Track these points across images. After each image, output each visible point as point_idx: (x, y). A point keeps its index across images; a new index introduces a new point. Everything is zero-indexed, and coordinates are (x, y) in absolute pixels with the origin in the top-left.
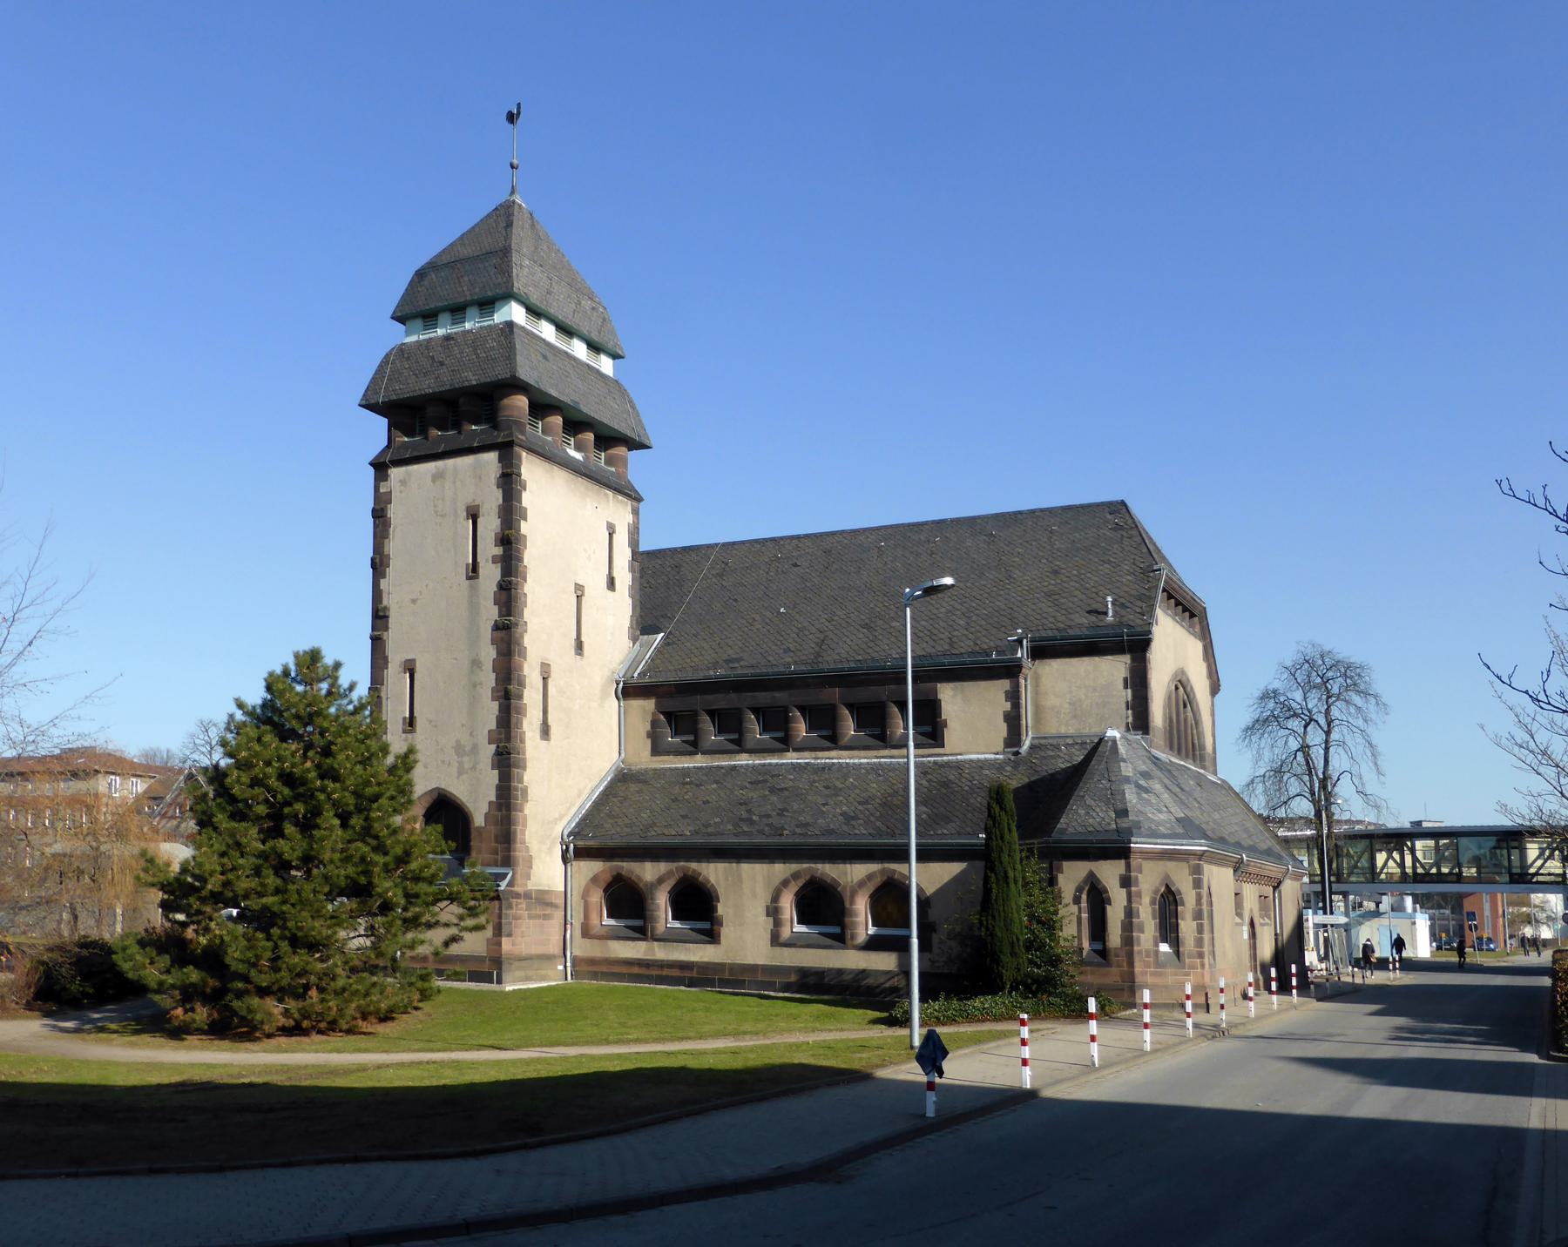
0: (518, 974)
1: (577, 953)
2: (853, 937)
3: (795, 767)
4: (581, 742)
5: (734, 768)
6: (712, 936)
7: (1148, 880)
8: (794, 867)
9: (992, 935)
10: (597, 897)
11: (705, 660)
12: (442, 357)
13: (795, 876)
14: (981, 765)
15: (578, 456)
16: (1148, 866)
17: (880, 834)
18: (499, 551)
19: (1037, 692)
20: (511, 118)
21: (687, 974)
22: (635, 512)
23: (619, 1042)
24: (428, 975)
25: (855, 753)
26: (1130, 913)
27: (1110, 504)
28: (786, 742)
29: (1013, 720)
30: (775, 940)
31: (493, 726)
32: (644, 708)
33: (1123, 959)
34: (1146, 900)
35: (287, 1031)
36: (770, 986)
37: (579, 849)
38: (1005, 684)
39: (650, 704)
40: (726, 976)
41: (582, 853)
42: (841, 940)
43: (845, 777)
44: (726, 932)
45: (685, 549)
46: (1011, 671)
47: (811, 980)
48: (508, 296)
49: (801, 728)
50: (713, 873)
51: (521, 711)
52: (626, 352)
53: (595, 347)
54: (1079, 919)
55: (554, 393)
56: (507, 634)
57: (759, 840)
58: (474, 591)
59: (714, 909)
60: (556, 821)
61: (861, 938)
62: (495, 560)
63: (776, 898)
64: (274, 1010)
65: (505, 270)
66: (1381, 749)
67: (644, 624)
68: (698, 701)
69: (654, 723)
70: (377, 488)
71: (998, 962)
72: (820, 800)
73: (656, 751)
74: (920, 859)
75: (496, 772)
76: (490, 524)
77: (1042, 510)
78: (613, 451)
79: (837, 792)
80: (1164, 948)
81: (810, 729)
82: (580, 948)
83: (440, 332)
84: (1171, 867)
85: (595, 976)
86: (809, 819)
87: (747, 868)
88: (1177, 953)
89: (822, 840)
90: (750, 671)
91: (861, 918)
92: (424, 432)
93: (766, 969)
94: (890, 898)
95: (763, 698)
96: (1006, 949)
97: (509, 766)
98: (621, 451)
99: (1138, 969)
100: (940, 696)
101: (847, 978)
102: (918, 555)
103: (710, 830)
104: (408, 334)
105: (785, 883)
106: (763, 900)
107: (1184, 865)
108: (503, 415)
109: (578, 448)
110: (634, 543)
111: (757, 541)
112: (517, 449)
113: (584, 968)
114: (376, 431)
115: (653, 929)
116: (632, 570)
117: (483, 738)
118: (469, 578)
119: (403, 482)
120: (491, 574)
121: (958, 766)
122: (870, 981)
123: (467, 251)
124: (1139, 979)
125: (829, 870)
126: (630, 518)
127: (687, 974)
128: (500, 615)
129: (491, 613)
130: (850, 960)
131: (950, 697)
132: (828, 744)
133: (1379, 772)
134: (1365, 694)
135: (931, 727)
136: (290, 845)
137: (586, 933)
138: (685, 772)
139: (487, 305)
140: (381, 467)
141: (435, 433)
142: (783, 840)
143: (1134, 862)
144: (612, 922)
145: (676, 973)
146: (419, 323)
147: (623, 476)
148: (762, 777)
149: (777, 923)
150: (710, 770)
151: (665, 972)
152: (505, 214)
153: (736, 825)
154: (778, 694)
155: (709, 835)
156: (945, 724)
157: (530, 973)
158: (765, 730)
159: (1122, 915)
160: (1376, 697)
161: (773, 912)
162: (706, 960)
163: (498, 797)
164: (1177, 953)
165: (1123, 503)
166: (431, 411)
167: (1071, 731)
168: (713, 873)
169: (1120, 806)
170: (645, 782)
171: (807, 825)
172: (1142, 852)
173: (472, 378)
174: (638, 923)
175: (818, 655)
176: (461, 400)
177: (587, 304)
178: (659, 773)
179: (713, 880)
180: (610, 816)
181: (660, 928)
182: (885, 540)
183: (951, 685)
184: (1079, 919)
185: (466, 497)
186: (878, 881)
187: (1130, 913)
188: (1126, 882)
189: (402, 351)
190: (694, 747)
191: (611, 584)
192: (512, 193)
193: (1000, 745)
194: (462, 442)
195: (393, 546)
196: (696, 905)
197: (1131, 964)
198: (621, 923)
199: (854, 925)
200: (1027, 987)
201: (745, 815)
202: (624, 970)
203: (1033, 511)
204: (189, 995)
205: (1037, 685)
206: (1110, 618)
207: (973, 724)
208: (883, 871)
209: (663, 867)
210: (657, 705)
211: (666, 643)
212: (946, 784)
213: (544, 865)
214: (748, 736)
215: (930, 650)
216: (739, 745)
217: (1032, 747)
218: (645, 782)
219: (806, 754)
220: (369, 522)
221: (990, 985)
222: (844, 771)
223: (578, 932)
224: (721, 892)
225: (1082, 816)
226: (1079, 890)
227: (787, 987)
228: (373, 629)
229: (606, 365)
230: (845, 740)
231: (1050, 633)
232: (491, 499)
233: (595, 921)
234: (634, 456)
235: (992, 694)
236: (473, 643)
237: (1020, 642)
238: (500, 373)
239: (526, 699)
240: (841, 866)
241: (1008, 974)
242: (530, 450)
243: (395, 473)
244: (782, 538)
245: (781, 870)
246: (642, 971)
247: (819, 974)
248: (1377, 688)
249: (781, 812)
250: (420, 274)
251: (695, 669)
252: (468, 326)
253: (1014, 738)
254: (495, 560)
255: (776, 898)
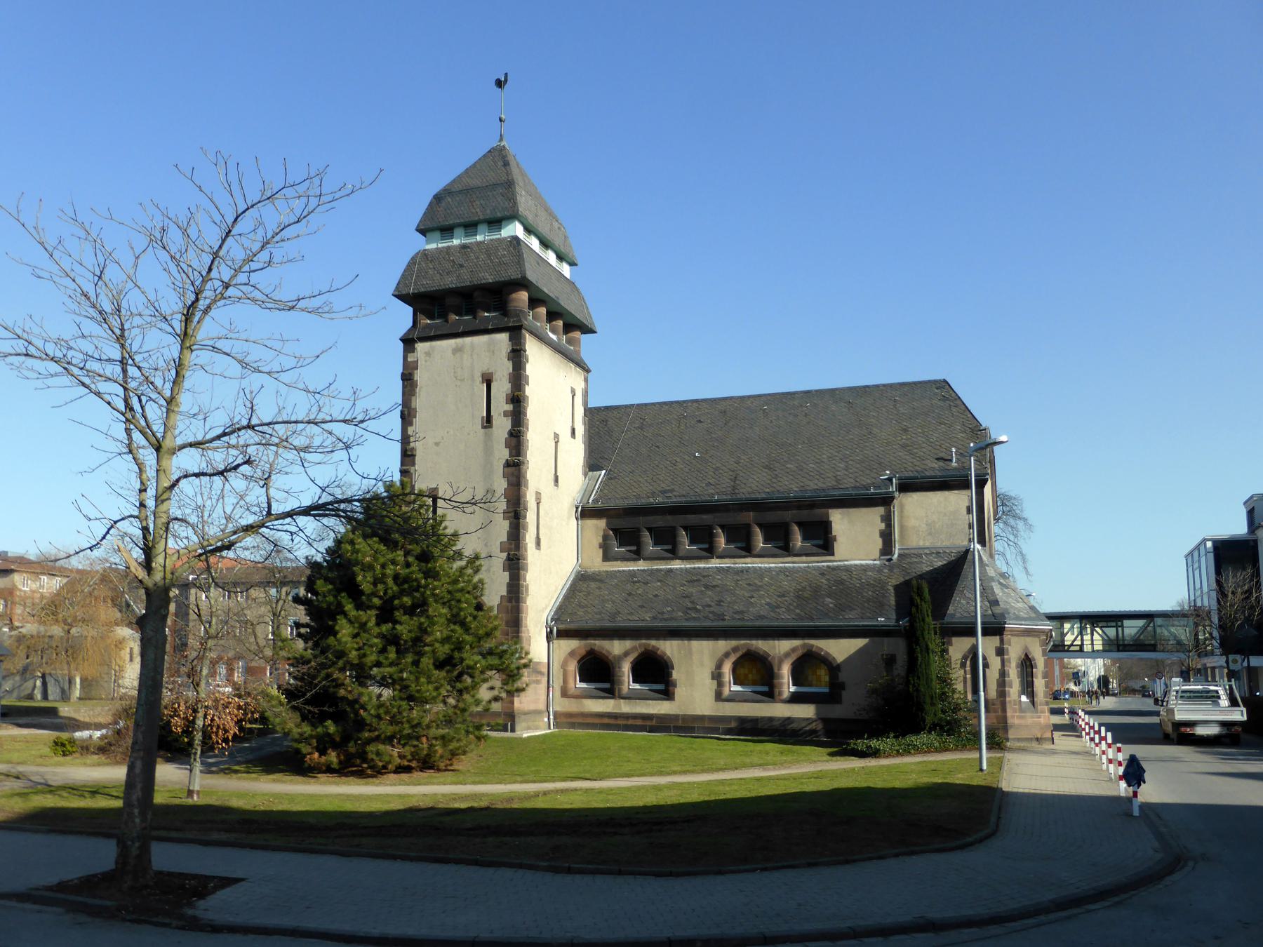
0: (524, 725)
1: (558, 709)
2: (780, 693)
3: (720, 570)
4: (558, 553)
5: (671, 570)
6: (667, 693)
7: (1014, 652)
8: (734, 643)
9: (918, 691)
10: (573, 667)
11: (644, 489)
12: (461, 261)
13: (735, 649)
14: (865, 569)
15: (554, 337)
16: (1014, 640)
17: (802, 619)
18: (510, 407)
19: (901, 517)
20: (499, 84)
21: (649, 723)
22: (586, 380)
23: (661, 773)
24: (482, 725)
25: (765, 559)
26: (1003, 674)
27: (935, 381)
28: (710, 552)
29: (887, 537)
30: (719, 697)
31: (505, 538)
32: (597, 526)
33: (998, 706)
34: (1013, 664)
35: (401, 769)
36: (716, 730)
37: (560, 630)
38: (877, 513)
39: (602, 523)
40: (680, 723)
41: (563, 634)
42: (770, 694)
43: (761, 577)
44: (679, 692)
45: (607, 408)
46: (885, 501)
47: (748, 726)
48: (514, 216)
49: (721, 541)
50: (669, 648)
51: (525, 528)
52: (578, 262)
53: (560, 258)
54: (965, 679)
55: (545, 290)
56: (515, 467)
57: (707, 624)
58: (488, 438)
59: (670, 675)
60: (543, 611)
61: (786, 695)
62: (506, 414)
63: (719, 666)
64: (394, 753)
65: (512, 199)
66: (1028, 557)
67: (592, 465)
68: (641, 521)
69: (605, 538)
70: (405, 358)
71: (922, 710)
72: (747, 595)
73: (607, 557)
74: (985, 633)
75: (507, 574)
76: (502, 388)
77: (884, 385)
78: (570, 335)
79: (758, 588)
80: (1024, 698)
81: (728, 542)
82: (560, 705)
83: (456, 242)
84: (1028, 639)
85: (573, 725)
86: (742, 608)
87: (696, 645)
88: (1033, 703)
89: (757, 623)
90: (684, 499)
91: (785, 680)
92: (443, 316)
93: (712, 719)
94: (805, 665)
95: (692, 519)
96: (928, 700)
97: (518, 569)
98: (577, 334)
99: (1009, 714)
100: (831, 519)
101: (776, 723)
102: (796, 416)
103: (666, 616)
104: (428, 242)
105: (727, 655)
106: (709, 667)
107: (1037, 639)
108: (512, 306)
109: (553, 331)
110: (585, 403)
111: (665, 403)
112: (524, 331)
113: (565, 720)
114: (404, 316)
115: (620, 690)
116: (584, 423)
117: (496, 549)
118: (484, 427)
119: (428, 354)
120: (502, 425)
121: (848, 569)
122: (794, 726)
123: (476, 182)
124: (1010, 721)
125: (761, 645)
126: (583, 385)
127: (649, 723)
128: (511, 455)
129: (503, 454)
130: (779, 710)
131: (840, 521)
132: (744, 553)
133: (1027, 573)
134: (1016, 517)
135: (822, 539)
136: (406, 627)
137: (565, 693)
138: (632, 574)
139: (496, 223)
140: (409, 342)
141: (453, 317)
142: (726, 623)
143: (1006, 637)
144: (584, 685)
145: (639, 722)
146: (437, 234)
147: (578, 353)
148: (695, 578)
149: (720, 684)
150: (652, 572)
151: (630, 722)
152: (499, 156)
153: (685, 613)
154: (704, 517)
155: (666, 620)
156: (835, 539)
157: (530, 724)
158: (692, 542)
159: (997, 676)
160: (1025, 520)
161: (717, 676)
162: (663, 712)
163: (509, 592)
164: (1033, 703)
165: (945, 381)
166: (450, 301)
167: (928, 544)
168: (669, 648)
169: (991, 598)
170: (601, 581)
171: (742, 612)
172: (1012, 630)
173: (488, 278)
174: (607, 686)
175: (734, 488)
176: (476, 294)
177: (556, 225)
178: (611, 575)
179: (668, 653)
180: (580, 606)
181: (625, 689)
182: (766, 404)
183: (840, 510)
184: (965, 679)
185: (483, 365)
186: (800, 653)
187: (1003, 674)
188: (1000, 652)
189: (425, 254)
190: (638, 555)
191: (488, 420)
192: (501, 139)
193: (877, 554)
194: (477, 324)
195: (419, 402)
196: (654, 672)
197: (1004, 710)
198: (592, 686)
199: (781, 685)
200: (942, 727)
201: (690, 605)
202: (597, 721)
203: (877, 386)
204: (323, 745)
205: (901, 512)
206: (954, 464)
207: (855, 539)
208: (804, 645)
209: (628, 644)
210: (607, 524)
211: (609, 477)
212: (842, 582)
213: (537, 645)
214: (681, 547)
215: (821, 485)
216: (673, 553)
217: (900, 555)
218: (601, 581)
219: (726, 560)
220: (399, 383)
221: (915, 726)
222: (761, 573)
223: (558, 693)
224: (675, 662)
225: (969, 604)
226: (965, 657)
227: (729, 731)
228: (402, 464)
229: (566, 270)
230: (757, 551)
231: (911, 474)
232: (503, 369)
233: (571, 684)
234: (585, 339)
235: (871, 518)
236: (488, 475)
237: (890, 480)
238: (513, 274)
239: (528, 519)
240: (771, 642)
241: (929, 719)
242: (531, 333)
243: (421, 347)
244: (684, 401)
245: (723, 645)
246: (612, 721)
247: (755, 720)
248: (1025, 515)
249: (719, 603)
250: (438, 198)
251: (638, 497)
252: (479, 238)
253: (887, 548)
254: (506, 414)
255: (719, 666)
